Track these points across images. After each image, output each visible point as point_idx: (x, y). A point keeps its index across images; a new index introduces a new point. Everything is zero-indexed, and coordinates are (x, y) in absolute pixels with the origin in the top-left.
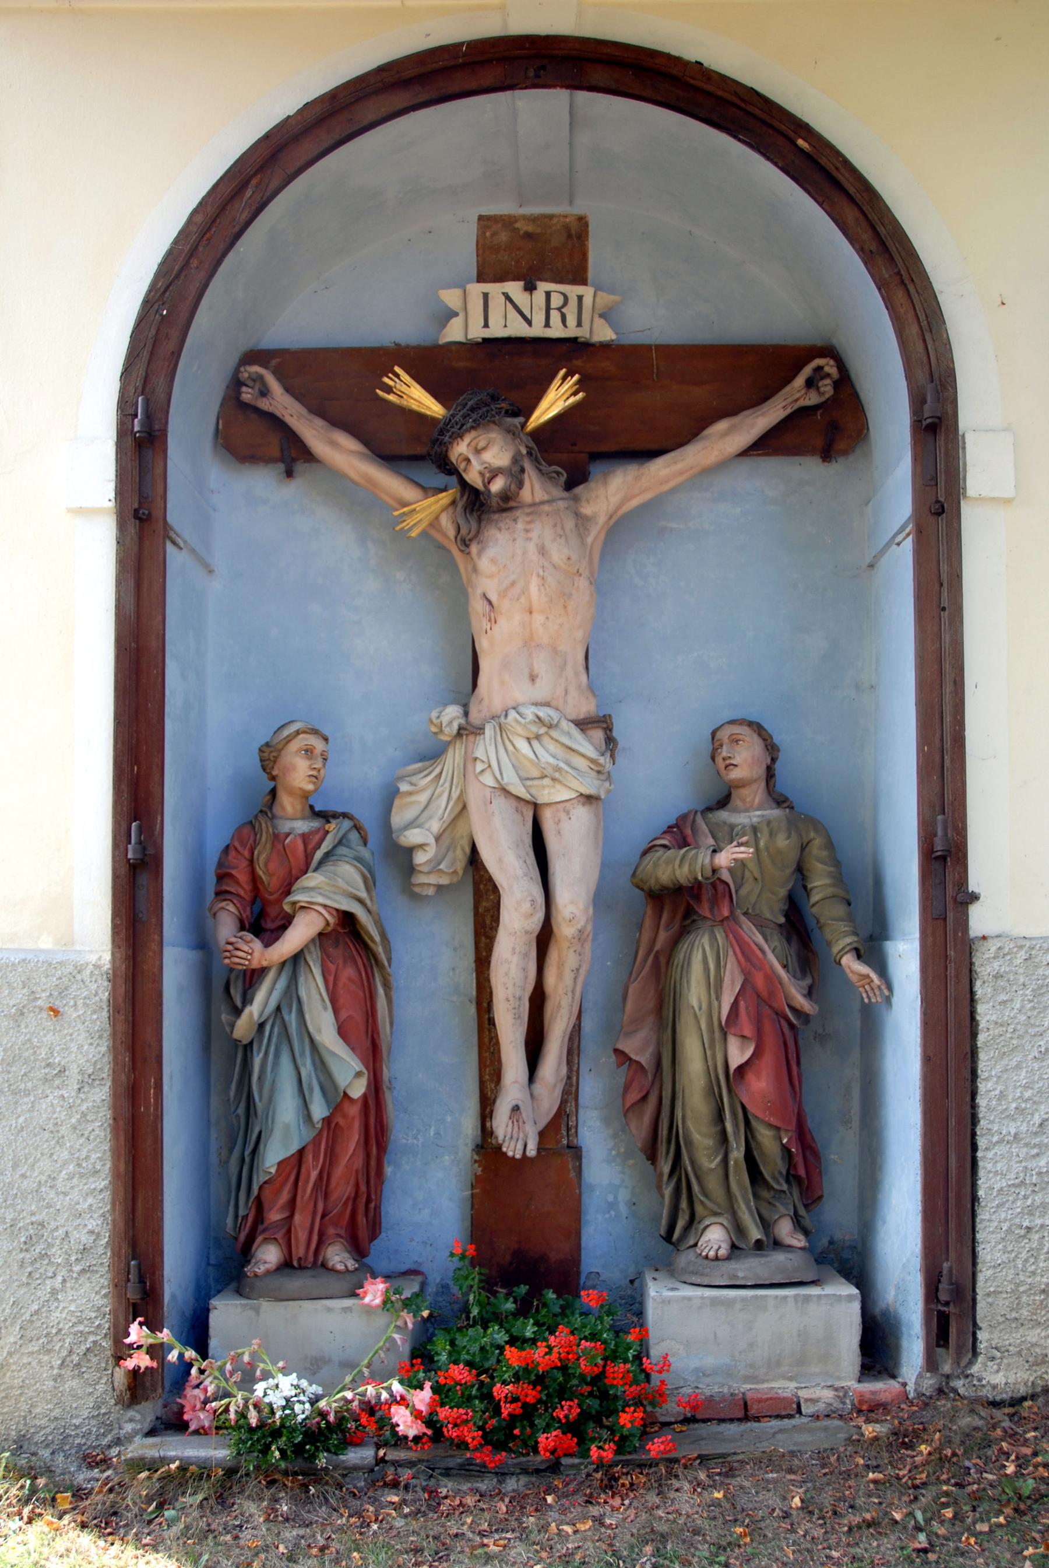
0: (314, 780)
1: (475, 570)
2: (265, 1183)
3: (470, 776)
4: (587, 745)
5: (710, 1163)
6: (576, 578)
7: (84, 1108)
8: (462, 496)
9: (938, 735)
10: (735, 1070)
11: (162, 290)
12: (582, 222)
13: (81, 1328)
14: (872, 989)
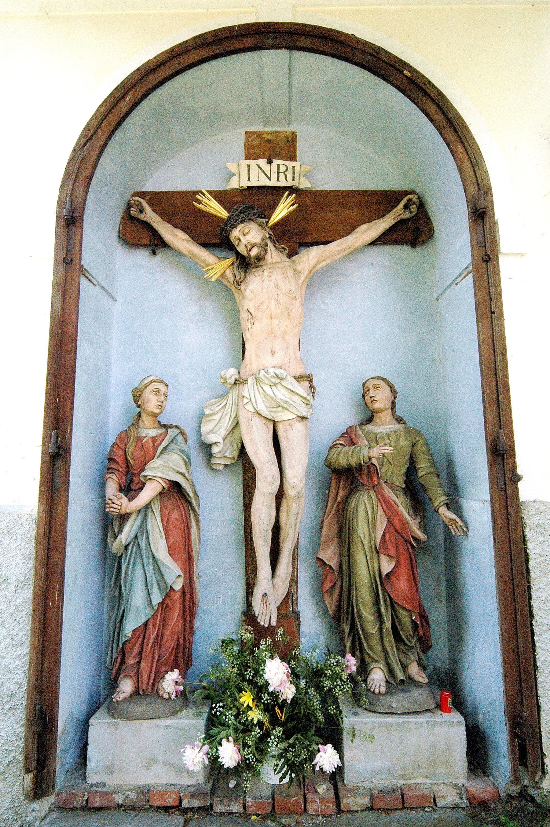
0: (160, 407)
1: (244, 298)
2: (126, 641)
3: (241, 406)
4: (302, 389)
5: (372, 629)
6: (294, 301)
7: (17, 603)
8: (237, 260)
9: (494, 383)
10: (385, 576)
11: (83, 144)
12: (294, 134)
13: (6, 747)
14: (457, 527)
